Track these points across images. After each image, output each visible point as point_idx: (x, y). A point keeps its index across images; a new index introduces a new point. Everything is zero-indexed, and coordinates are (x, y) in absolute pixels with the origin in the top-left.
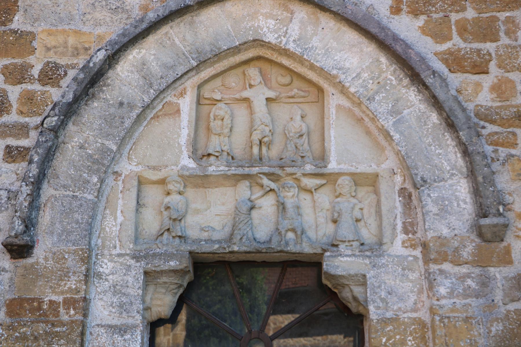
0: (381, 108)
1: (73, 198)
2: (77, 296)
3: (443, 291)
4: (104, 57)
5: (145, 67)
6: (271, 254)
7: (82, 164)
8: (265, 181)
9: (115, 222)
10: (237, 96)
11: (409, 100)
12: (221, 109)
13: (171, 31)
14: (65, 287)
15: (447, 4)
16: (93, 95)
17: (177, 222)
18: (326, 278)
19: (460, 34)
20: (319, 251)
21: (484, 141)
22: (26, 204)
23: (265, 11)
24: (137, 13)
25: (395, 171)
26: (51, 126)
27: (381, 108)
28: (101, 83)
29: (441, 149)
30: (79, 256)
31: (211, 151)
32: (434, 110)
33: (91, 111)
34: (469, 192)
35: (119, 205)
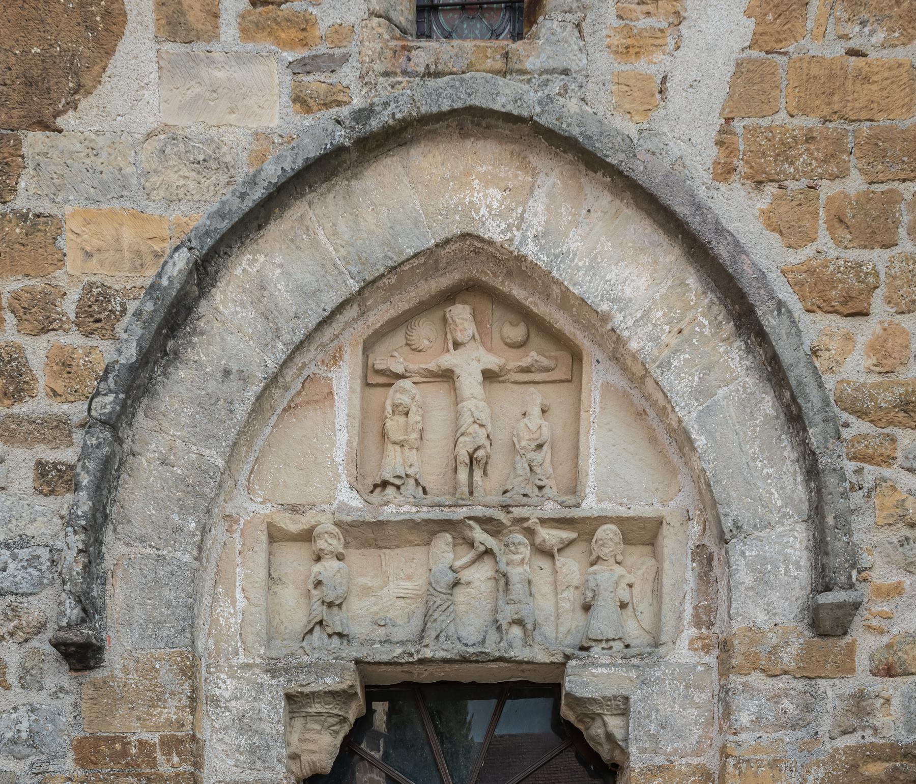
0: (680, 383)
1: (157, 560)
2: (180, 734)
3: (745, 718)
4: (187, 264)
5: (265, 293)
6: (485, 665)
7: (167, 496)
8: (479, 534)
9: (234, 608)
10: (432, 366)
11: (729, 367)
12: (403, 391)
13: (311, 213)
14: (160, 717)
15: (816, 159)
16: (176, 353)
17: (335, 609)
18: (567, 705)
19: (831, 229)
20: (559, 659)
22: (78, 568)
23: (485, 168)
24: (244, 171)
25: (690, 514)
26: (104, 414)
27: (680, 383)
28: (188, 328)
29: (772, 467)
30: (178, 665)
31: (388, 476)
32: (769, 389)
33: (175, 388)
34: (807, 547)
35: (238, 578)
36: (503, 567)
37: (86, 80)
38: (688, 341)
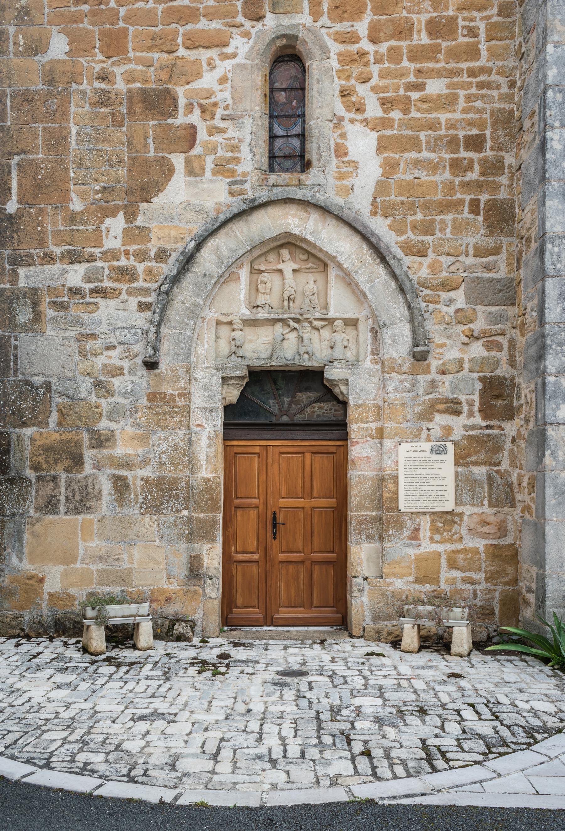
3: (390, 389)
8: (292, 323)
10: (275, 268)
19: (412, 230)
21: (420, 299)
24: (212, 214)
31: (259, 304)
36: (301, 334)
37: (161, 188)
38: (364, 265)
